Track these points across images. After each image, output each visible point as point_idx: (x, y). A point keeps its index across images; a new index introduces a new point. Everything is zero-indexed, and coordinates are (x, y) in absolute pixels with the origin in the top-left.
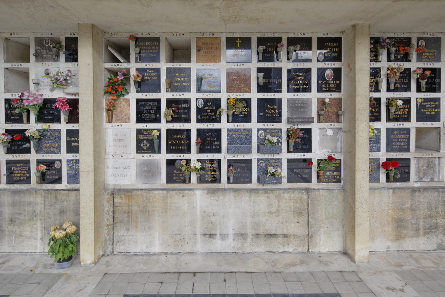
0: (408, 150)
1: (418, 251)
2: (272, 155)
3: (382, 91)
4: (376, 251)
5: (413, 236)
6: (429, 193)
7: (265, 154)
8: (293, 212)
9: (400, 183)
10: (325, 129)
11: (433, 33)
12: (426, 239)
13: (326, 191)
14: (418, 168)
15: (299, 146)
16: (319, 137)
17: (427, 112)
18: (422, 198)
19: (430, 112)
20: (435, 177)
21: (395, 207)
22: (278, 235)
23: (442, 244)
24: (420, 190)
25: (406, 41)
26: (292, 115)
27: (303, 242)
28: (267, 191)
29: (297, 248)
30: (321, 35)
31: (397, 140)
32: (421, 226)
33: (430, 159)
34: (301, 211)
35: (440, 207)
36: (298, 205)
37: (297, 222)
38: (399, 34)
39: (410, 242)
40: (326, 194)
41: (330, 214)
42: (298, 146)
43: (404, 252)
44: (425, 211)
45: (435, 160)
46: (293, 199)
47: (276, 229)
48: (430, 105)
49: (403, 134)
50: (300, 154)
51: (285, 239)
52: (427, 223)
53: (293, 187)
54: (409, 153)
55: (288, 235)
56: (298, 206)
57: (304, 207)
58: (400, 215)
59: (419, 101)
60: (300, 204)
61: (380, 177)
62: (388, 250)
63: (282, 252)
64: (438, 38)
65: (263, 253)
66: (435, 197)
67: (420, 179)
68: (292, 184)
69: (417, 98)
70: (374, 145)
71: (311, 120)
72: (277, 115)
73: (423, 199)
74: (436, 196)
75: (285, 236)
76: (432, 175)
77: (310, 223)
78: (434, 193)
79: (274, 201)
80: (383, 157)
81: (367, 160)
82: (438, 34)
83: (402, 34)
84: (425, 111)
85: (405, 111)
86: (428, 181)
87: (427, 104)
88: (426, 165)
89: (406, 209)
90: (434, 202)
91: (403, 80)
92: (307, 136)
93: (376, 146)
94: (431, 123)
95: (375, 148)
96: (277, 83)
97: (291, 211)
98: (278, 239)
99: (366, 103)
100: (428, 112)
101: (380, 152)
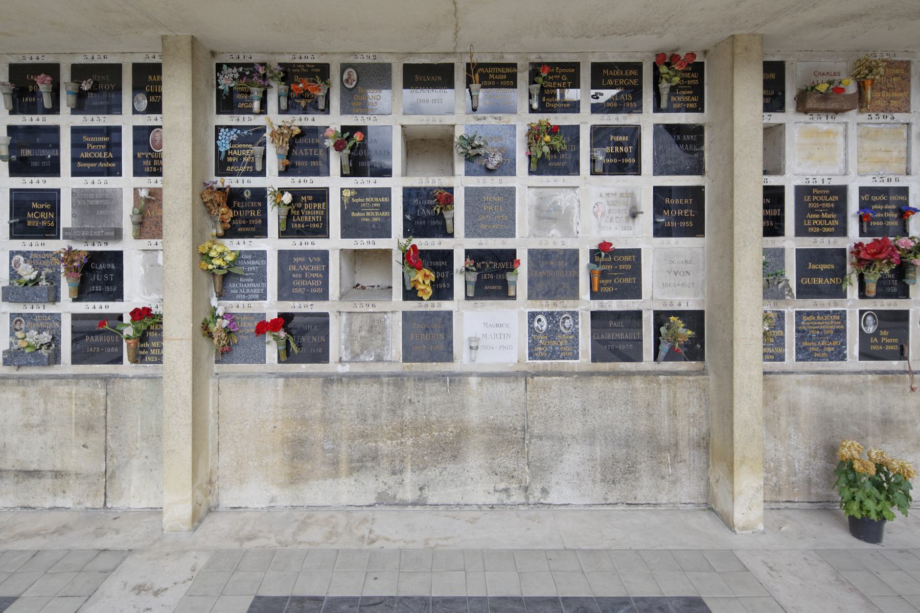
0: (324, 296)
1: (335, 508)
2: (41, 305)
3: (269, 174)
4: (247, 507)
5: (325, 477)
6: (361, 385)
7: (25, 304)
8: (75, 425)
9: (308, 365)
10: (155, 253)
11: (374, 54)
12: (353, 483)
13: (145, 380)
14: (350, 333)
15: (97, 287)
16: (142, 269)
17: (363, 217)
18: (345, 396)
19: (370, 217)
20: (386, 352)
21: (290, 414)
22: (44, 473)
23: (388, 494)
24: (341, 380)
25: (318, 70)
26: (83, 224)
27: (94, 488)
28: (22, 381)
29: (81, 500)
30: (140, 59)
31: (300, 276)
32: (343, 456)
33: (374, 315)
34: (91, 423)
35: (384, 415)
36: (86, 410)
37: (84, 446)
38: (303, 56)
39: (320, 489)
40: (144, 388)
41: (152, 428)
42: (95, 288)
43: (307, 508)
44: (352, 423)
45: (386, 316)
46: (75, 398)
47: (38, 460)
48: (368, 202)
49: (314, 263)
50: (98, 304)
51: (58, 482)
52: (355, 447)
53: (83, 373)
54: (326, 303)
55: (63, 473)
56: (86, 413)
57: (97, 414)
58: (300, 431)
59: (347, 194)
60: (89, 408)
61: (265, 352)
62: (272, 505)
63: (50, 509)
64: (384, 64)
65: (12, 510)
66: (373, 394)
67: (353, 358)
68: (82, 366)
69: (342, 189)
70: (254, 285)
71: (107, 234)
72: (50, 223)
73: (348, 397)
74: (376, 393)
75: (58, 474)
76: (378, 348)
77: (109, 449)
78: (372, 386)
79: (36, 401)
80: (272, 311)
81: (187, 317)
82: (384, 56)
83: (310, 56)
84: (358, 214)
85: (316, 215)
86: (371, 361)
87: (363, 200)
88: (366, 328)
89: (311, 419)
90: (371, 405)
91: (313, 152)
92: (113, 267)
93: (257, 288)
94: (371, 240)
95: (255, 291)
96: (49, 156)
97: (71, 423)
98: (43, 480)
99: (183, 198)
100: (365, 217)
101: (265, 299)
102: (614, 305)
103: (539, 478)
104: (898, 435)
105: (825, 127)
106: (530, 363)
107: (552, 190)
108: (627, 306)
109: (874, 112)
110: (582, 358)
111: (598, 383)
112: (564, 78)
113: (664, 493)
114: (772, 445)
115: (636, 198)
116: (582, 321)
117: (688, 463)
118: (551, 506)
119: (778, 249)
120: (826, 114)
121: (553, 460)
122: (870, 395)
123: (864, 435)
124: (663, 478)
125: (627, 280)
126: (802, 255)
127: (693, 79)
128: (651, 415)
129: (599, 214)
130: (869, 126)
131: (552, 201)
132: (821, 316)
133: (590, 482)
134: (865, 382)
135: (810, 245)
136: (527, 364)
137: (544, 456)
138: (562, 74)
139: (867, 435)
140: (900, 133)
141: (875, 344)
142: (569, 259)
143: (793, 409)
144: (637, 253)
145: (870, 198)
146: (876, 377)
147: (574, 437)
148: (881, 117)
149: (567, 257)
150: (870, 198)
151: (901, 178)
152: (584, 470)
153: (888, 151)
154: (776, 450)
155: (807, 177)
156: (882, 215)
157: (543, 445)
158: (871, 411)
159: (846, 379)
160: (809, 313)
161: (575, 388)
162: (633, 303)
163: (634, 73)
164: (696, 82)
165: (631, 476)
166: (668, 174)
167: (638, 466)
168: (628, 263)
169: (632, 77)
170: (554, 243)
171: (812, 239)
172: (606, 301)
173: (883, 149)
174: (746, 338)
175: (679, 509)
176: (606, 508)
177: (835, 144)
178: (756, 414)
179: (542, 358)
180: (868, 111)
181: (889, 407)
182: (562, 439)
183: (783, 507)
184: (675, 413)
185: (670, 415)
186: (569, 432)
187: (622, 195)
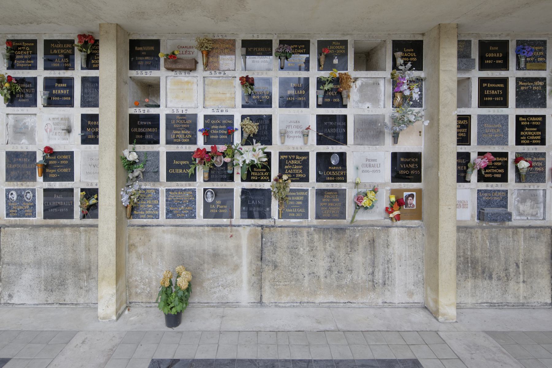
102: (57, 185)
103: (7, 288)
104: (222, 263)
105: (186, 79)
106: (7, 220)
107: (23, 116)
108: (65, 186)
109: (213, 70)
110: (38, 216)
111: (44, 232)
112: (28, 49)
113: (82, 297)
114: (147, 269)
115: (70, 121)
116: (38, 194)
117: (96, 279)
118: (14, 305)
119: (156, 152)
120: (185, 71)
121: (15, 277)
122: (206, 239)
123: (202, 263)
124: (81, 288)
125: (65, 170)
126: (170, 155)
127: (341, 49)
128: (75, 251)
129: (48, 130)
130: (213, 78)
131: (23, 122)
132: (181, 192)
133: (38, 291)
134: (203, 231)
135: (175, 150)
136: (5, 220)
137: (10, 275)
138: (27, 46)
139: (204, 263)
140: (232, 83)
141: (213, 209)
142: (31, 157)
143: (160, 247)
144: (71, 154)
145: (210, 121)
146: (210, 228)
147: (28, 264)
148: (218, 73)
149: (29, 156)
150: (210, 121)
151: (229, 110)
152: (34, 283)
153: (224, 94)
154: (149, 272)
155: (173, 109)
156: (217, 132)
157: (10, 268)
158: (206, 249)
159: (192, 229)
160: (173, 191)
161: (30, 235)
162: (69, 184)
163: (70, 46)
164: (344, 51)
165: (62, 287)
166: (89, 107)
167: (67, 281)
168: (66, 160)
169: (68, 48)
170: (22, 148)
171: (176, 146)
172: (52, 183)
173: (221, 92)
174: (105, 205)
175: (90, 307)
176: (47, 306)
177: (192, 89)
178: (111, 250)
179: (14, 217)
180: (210, 69)
181: (218, 247)
182: (21, 265)
183: (154, 306)
184: (89, 250)
185: (86, 250)
186: (26, 261)
187: (62, 119)
